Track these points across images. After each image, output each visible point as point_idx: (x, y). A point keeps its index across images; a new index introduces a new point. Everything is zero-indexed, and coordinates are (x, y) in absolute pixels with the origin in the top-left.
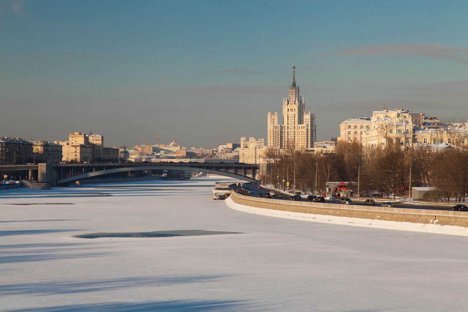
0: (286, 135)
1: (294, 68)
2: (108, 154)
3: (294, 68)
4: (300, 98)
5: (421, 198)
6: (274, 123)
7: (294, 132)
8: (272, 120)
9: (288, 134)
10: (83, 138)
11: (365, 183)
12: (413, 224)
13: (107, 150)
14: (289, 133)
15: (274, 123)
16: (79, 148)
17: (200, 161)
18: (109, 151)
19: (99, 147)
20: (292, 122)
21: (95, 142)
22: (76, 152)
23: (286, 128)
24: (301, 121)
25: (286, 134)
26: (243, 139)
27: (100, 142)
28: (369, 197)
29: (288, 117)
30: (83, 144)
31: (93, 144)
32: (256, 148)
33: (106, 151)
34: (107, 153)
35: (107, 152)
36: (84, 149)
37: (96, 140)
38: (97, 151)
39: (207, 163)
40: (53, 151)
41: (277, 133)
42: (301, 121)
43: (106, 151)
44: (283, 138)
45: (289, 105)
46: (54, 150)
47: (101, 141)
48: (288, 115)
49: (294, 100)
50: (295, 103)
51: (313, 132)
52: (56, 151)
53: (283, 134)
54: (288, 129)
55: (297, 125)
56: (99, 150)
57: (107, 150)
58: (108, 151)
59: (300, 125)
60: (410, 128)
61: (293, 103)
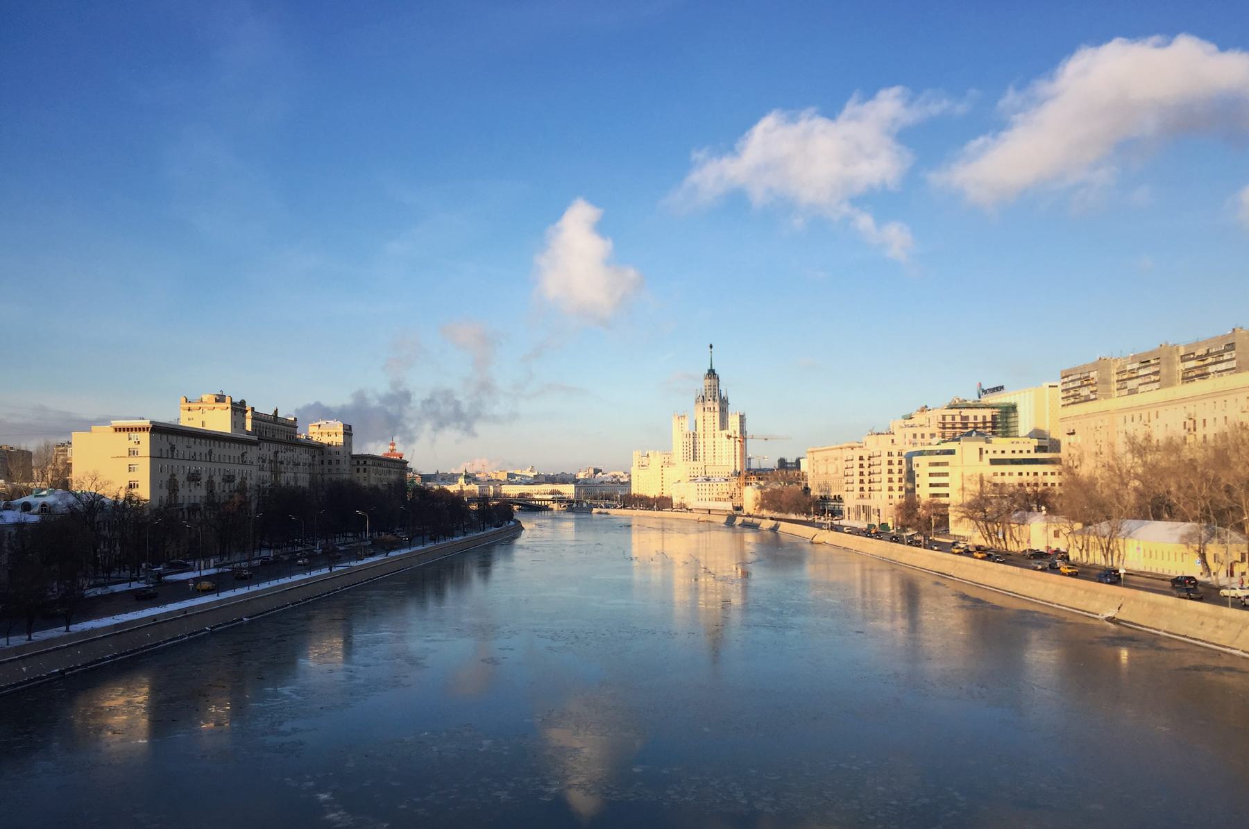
0: (702, 448)
1: (711, 347)
2: (365, 470)
3: (711, 347)
5: (233, 401)
7: (714, 442)
9: (704, 446)
10: (230, 410)
13: (362, 462)
14: (706, 444)
16: (145, 437)
18: (368, 463)
19: (338, 453)
21: (325, 440)
22: (133, 453)
23: (701, 436)
24: (742, 419)
25: (702, 444)
27: (339, 440)
28: (731, 529)
29: (704, 420)
30: (229, 431)
33: (358, 462)
36: (164, 442)
37: (329, 434)
38: (330, 462)
39: (507, 539)
40: (299, 465)
41: (688, 445)
42: (723, 424)
43: (358, 462)
44: (698, 452)
46: (268, 458)
47: (342, 436)
49: (712, 394)
50: (714, 400)
52: (299, 464)
53: (697, 445)
54: (704, 437)
55: (718, 431)
56: (338, 462)
57: (362, 462)
58: (365, 462)
60: (1063, 406)
61: (711, 399)
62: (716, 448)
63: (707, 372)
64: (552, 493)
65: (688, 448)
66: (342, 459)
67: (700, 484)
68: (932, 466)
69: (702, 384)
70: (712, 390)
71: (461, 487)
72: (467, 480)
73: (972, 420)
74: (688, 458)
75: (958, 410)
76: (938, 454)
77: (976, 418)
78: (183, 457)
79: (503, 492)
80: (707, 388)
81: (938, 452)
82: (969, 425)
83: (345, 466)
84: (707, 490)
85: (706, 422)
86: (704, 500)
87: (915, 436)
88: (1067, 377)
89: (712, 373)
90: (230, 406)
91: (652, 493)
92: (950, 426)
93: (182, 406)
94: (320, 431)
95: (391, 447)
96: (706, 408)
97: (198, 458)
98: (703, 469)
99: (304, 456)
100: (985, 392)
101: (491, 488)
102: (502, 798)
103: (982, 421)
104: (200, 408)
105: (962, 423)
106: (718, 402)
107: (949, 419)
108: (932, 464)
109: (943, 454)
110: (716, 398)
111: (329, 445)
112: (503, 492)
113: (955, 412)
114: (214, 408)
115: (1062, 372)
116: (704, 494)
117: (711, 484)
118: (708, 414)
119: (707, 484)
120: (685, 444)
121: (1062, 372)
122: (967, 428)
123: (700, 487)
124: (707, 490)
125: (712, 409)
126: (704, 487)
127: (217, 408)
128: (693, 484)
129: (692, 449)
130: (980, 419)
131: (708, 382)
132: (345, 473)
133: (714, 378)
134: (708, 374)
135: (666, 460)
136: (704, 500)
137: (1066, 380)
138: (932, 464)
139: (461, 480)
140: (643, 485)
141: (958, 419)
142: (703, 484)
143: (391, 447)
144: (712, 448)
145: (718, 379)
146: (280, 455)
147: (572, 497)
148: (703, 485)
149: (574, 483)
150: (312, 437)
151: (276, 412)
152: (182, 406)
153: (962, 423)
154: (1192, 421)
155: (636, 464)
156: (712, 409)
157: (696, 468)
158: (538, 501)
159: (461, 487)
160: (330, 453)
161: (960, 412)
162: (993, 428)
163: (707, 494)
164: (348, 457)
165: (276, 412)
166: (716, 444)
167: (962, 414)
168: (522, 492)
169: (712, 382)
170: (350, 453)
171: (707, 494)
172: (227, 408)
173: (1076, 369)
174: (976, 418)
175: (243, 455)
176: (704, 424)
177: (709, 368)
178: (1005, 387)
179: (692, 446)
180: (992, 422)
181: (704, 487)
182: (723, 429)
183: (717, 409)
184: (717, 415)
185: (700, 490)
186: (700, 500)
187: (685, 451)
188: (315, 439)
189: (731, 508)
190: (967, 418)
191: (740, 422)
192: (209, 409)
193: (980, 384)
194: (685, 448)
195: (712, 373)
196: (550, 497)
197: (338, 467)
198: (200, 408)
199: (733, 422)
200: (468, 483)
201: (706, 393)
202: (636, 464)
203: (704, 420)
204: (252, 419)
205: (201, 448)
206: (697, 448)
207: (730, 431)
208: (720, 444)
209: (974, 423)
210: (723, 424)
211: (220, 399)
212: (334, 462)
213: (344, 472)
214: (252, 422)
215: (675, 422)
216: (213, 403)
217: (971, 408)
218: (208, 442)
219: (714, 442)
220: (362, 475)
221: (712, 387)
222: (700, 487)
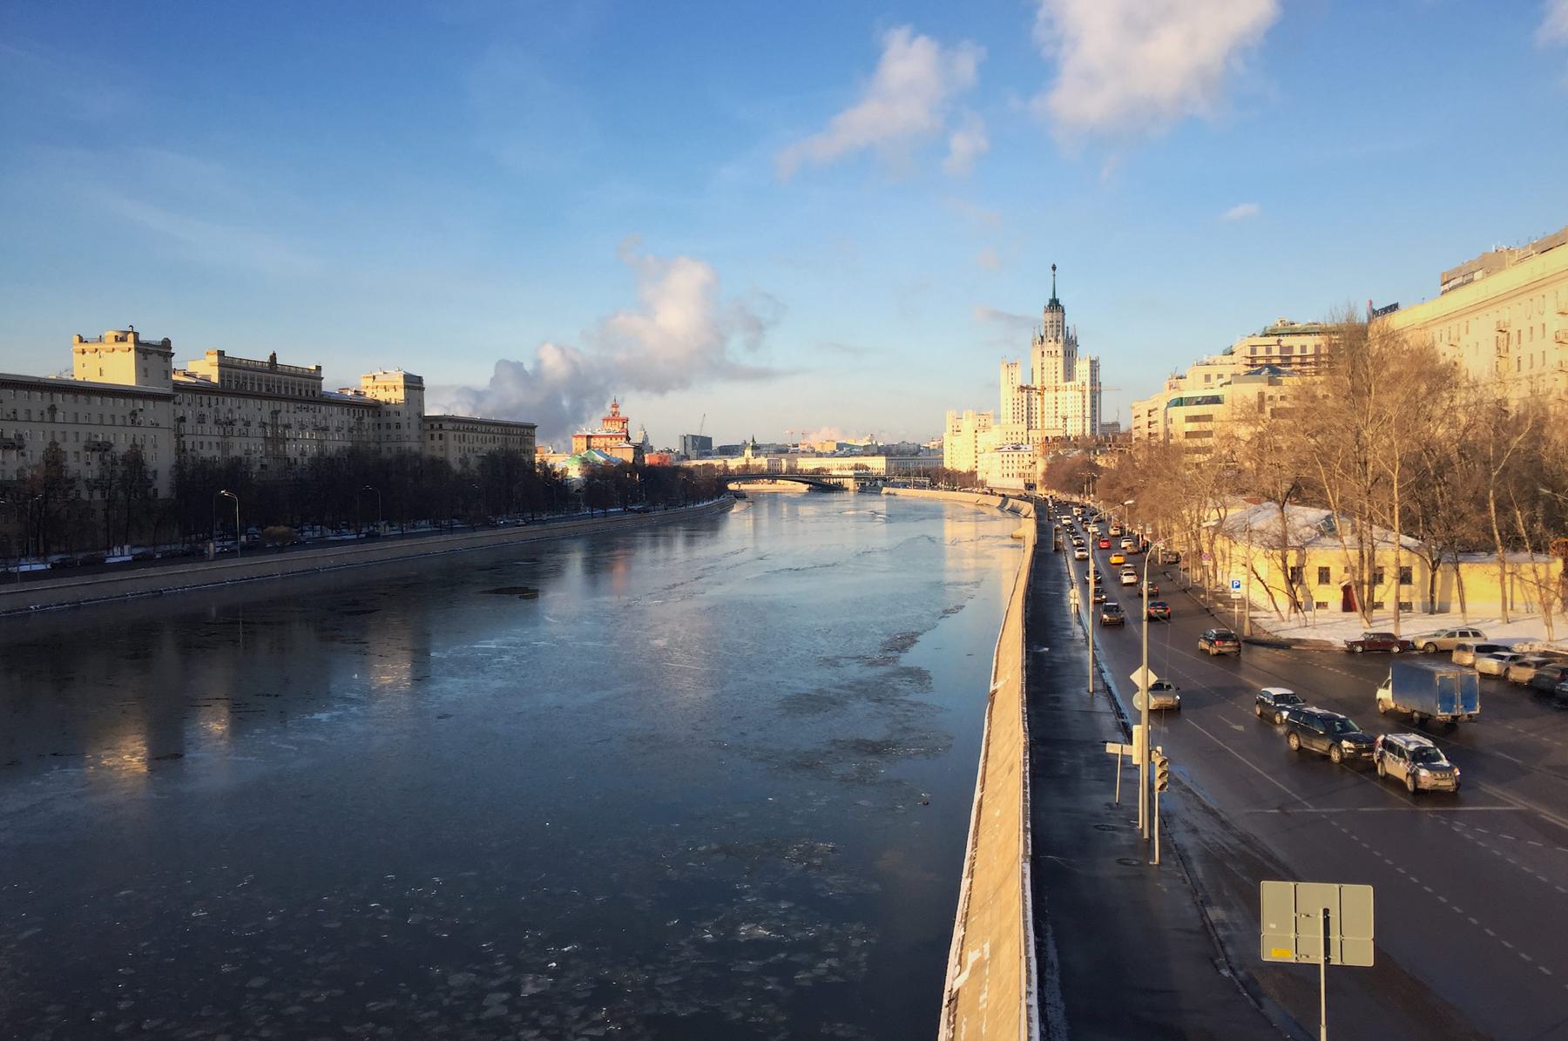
1: (1054, 268)
3: (1054, 268)
4: (1066, 330)
5: (141, 338)
6: (1013, 381)
7: (1056, 398)
8: (1010, 374)
10: (133, 351)
11: (1362, 507)
12: (1331, 576)
15: (1013, 381)
17: (1311, 637)
20: (1051, 373)
21: (382, 396)
24: (1094, 366)
26: (950, 415)
27: (398, 396)
29: (1043, 368)
30: (134, 384)
31: (378, 401)
32: (976, 431)
33: (432, 426)
34: (436, 435)
35: (437, 429)
41: (1020, 402)
42: (1069, 374)
43: (432, 426)
45: (1045, 344)
48: (1042, 364)
49: (1055, 334)
50: (1056, 340)
51: (1095, 397)
55: (1061, 383)
56: (398, 426)
59: (1069, 384)
61: (1053, 340)
62: (1059, 405)
63: (1048, 303)
64: (856, 467)
65: (1020, 406)
66: (404, 423)
67: (1006, 454)
68: (1191, 421)
69: (1041, 316)
70: (1055, 327)
71: (747, 460)
72: (755, 452)
73: (1297, 352)
74: (1020, 420)
75: (1276, 338)
76: (1198, 403)
77: (1303, 348)
78: (64, 419)
79: (798, 467)
80: (1048, 324)
81: (1199, 399)
82: (1293, 360)
83: (413, 432)
84: (1016, 462)
85: (1045, 370)
86: (1010, 475)
87: (1208, 378)
88: (1448, 282)
89: (1055, 305)
90: (132, 346)
91: (964, 467)
92: (1299, 360)
93: (75, 348)
94: (376, 384)
95: (614, 410)
96: (1045, 352)
97: (108, 420)
98: (1025, 433)
99: (337, 417)
100: (1375, 313)
101: (784, 462)
102: (1092, 777)
103: (1313, 352)
104: (96, 350)
105: (1281, 357)
106: (1062, 343)
107: (1261, 352)
108: (1190, 419)
109: (1206, 403)
110: (1059, 338)
111: (387, 403)
112: (798, 467)
113: (1272, 340)
114: (113, 350)
115: (1443, 274)
116: (1010, 468)
117: (1021, 454)
118: (1048, 360)
119: (1016, 454)
120: (1016, 401)
121: (1443, 274)
122: (1289, 365)
123: (1005, 459)
124: (1016, 462)
125: (1053, 353)
126: (1010, 459)
127: (118, 349)
128: (997, 455)
129: (1025, 408)
130: (1310, 351)
131: (1049, 317)
132: (412, 442)
133: (1057, 311)
134: (1049, 306)
135: (982, 423)
136: (1010, 475)
137: (1447, 287)
138: (1190, 419)
139: (748, 452)
140: (956, 459)
141: (1276, 351)
142: (1010, 454)
143: (614, 410)
144: (1053, 405)
145: (1063, 311)
146: (283, 418)
147: (883, 473)
148: (1010, 456)
149: (886, 455)
150: (365, 393)
151: (273, 357)
152: (75, 348)
153: (1281, 357)
154: (1505, 335)
155: (949, 429)
156: (1053, 353)
157: (1015, 433)
158: (836, 478)
159: (747, 460)
160: (388, 414)
161: (1279, 341)
162: (1330, 363)
163: (1016, 468)
164: (415, 421)
165: (273, 357)
166: (1059, 401)
167: (1282, 343)
168: (818, 467)
169: (1055, 317)
170: (420, 414)
171: (1016, 468)
172: (130, 349)
173: (1459, 270)
174: (1303, 348)
175: (134, 414)
176: (1042, 373)
177: (1052, 298)
178: (1400, 306)
179: (1025, 404)
180: (1328, 354)
181: (1010, 459)
182: (1069, 380)
183: (1061, 353)
184: (1060, 361)
185: (1011, 462)
186: (1005, 476)
187: (1016, 411)
188: (369, 396)
189: (1022, 486)
190: (1290, 348)
191: (1091, 370)
192: (107, 352)
193: (1371, 303)
194: (1015, 406)
195: (1055, 305)
196: (851, 473)
197: (398, 432)
198: (96, 350)
199: (1082, 369)
200: (756, 456)
201: (1046, 331)
202: (949, 429)
203: (1043, 368)
204: (219, 366)
205: (39, 401)
206: (1033, 406)
207: (1078, 382)
208: (1064, 401)
209: (1301, 356)
210: (1069, 374)
211: (121, 339)
212: (393, 426)
213: (407, 439)
214: (220, 371)
215: (1003, 376)
216: (111, 343)
217: (1298, 334)
218: (346, 409)
219: (1056, 398)
220: (437, 443)
221: (1055, 324)
222: (1005, 459)
